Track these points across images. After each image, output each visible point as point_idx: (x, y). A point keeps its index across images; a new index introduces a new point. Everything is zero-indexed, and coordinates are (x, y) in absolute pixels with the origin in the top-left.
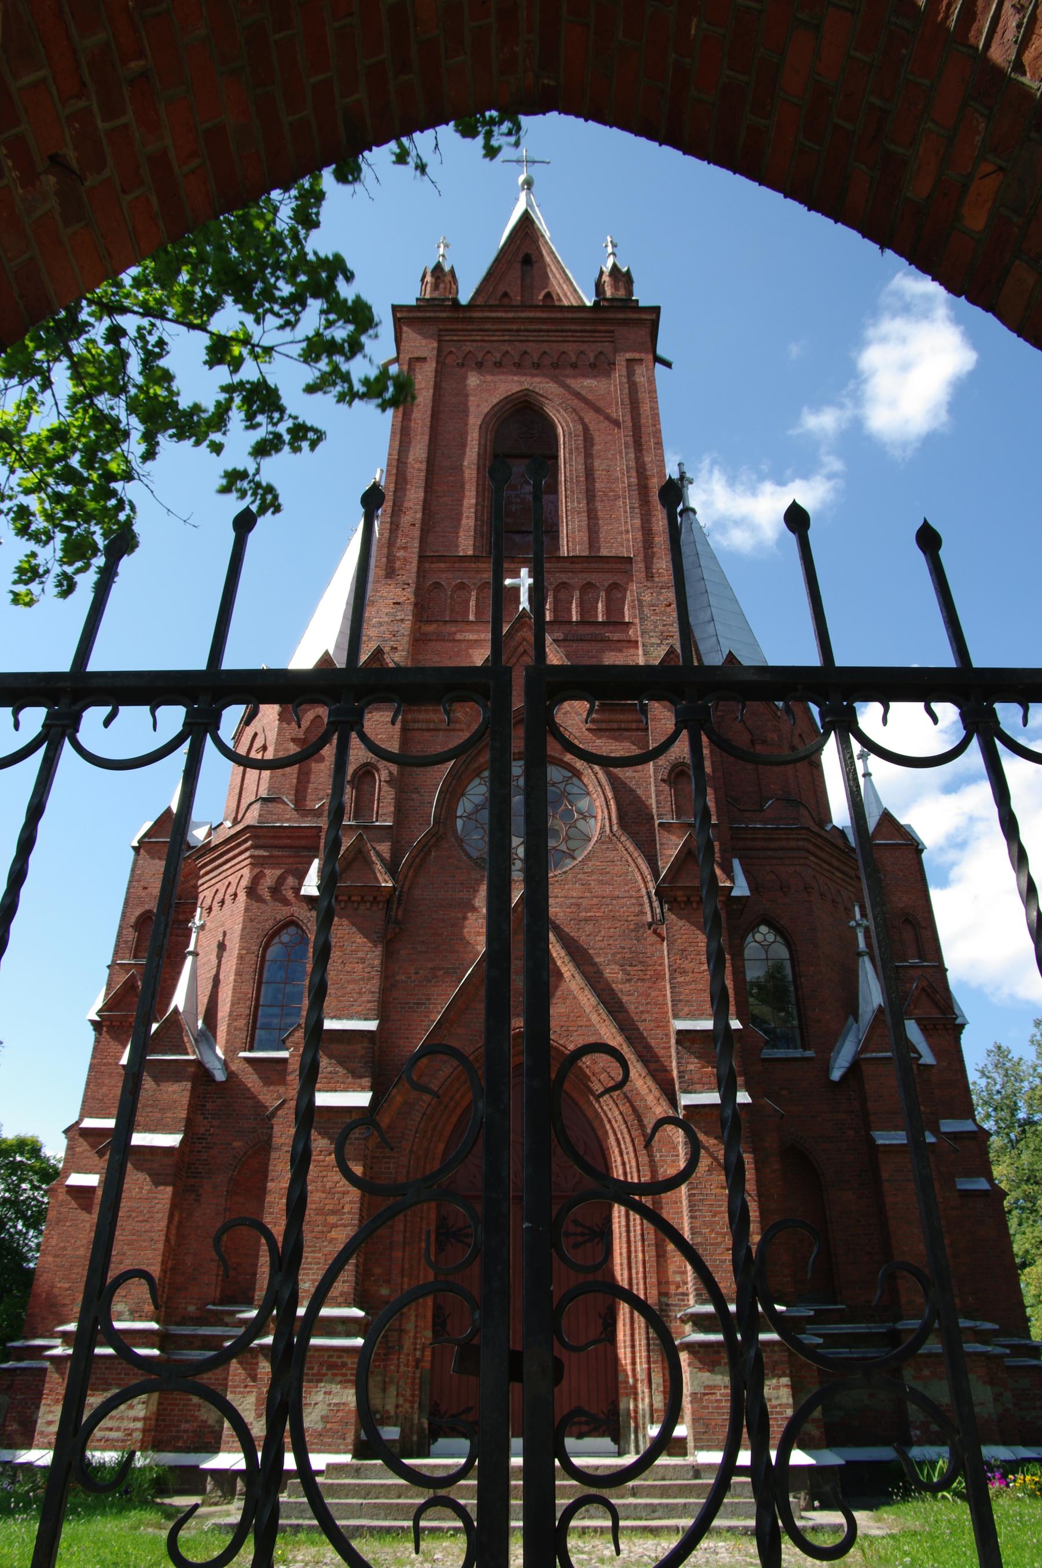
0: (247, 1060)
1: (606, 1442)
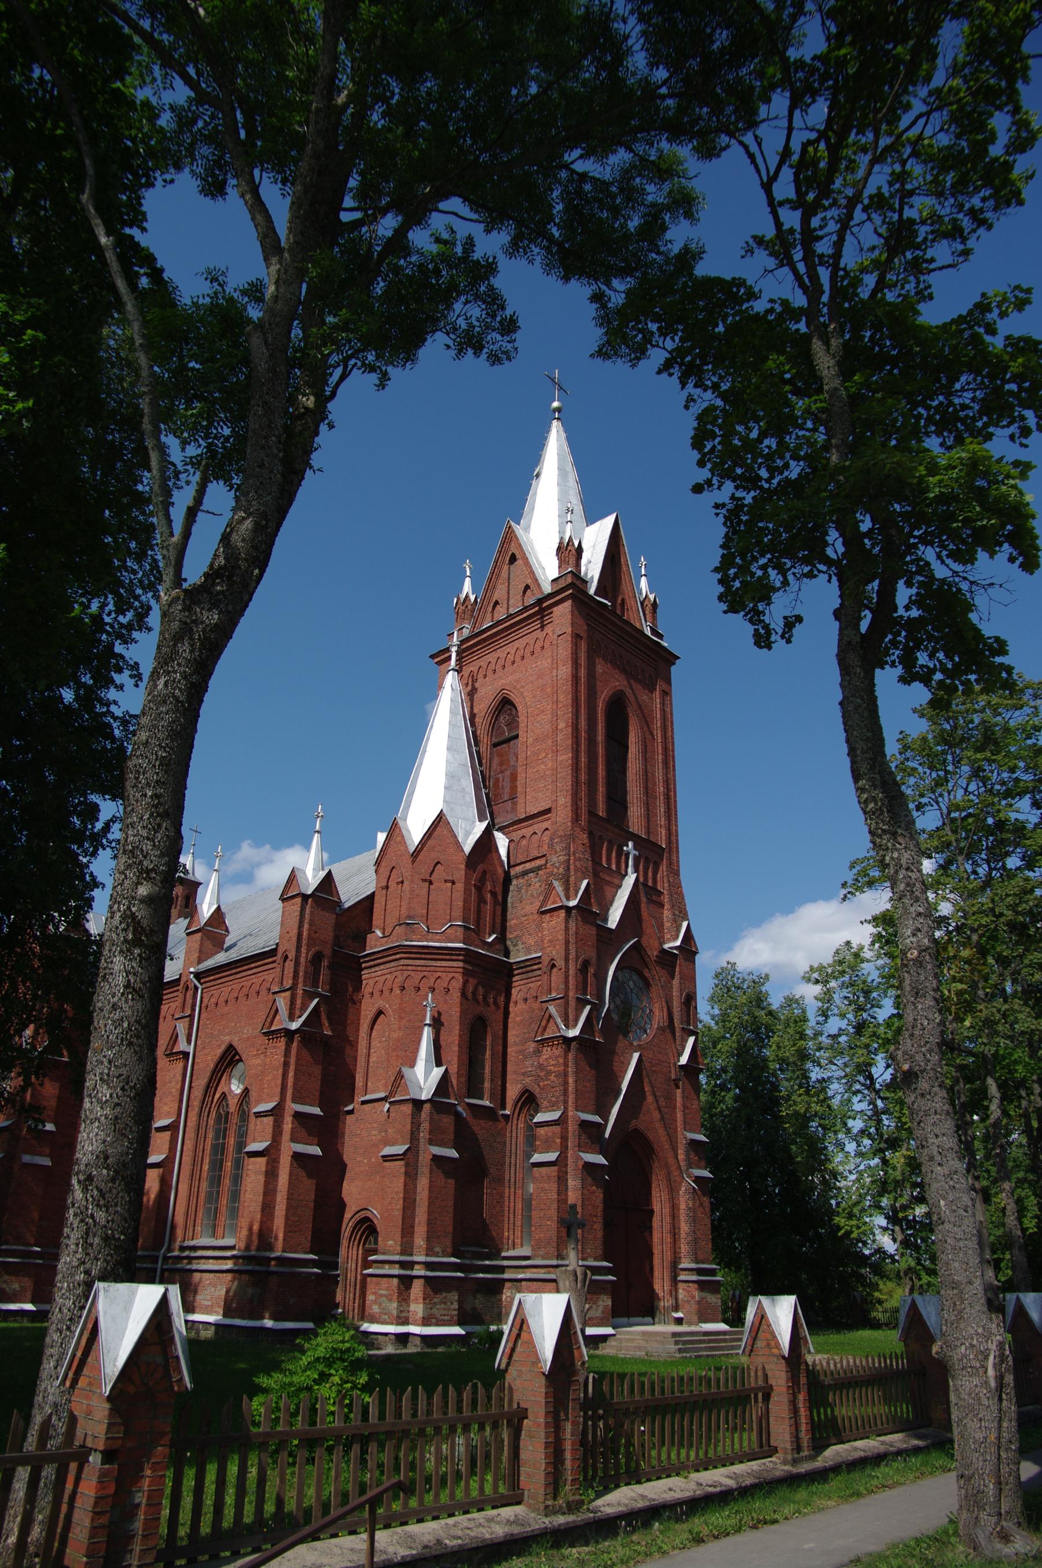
0: (468, 1104)
1: (650, 1319)
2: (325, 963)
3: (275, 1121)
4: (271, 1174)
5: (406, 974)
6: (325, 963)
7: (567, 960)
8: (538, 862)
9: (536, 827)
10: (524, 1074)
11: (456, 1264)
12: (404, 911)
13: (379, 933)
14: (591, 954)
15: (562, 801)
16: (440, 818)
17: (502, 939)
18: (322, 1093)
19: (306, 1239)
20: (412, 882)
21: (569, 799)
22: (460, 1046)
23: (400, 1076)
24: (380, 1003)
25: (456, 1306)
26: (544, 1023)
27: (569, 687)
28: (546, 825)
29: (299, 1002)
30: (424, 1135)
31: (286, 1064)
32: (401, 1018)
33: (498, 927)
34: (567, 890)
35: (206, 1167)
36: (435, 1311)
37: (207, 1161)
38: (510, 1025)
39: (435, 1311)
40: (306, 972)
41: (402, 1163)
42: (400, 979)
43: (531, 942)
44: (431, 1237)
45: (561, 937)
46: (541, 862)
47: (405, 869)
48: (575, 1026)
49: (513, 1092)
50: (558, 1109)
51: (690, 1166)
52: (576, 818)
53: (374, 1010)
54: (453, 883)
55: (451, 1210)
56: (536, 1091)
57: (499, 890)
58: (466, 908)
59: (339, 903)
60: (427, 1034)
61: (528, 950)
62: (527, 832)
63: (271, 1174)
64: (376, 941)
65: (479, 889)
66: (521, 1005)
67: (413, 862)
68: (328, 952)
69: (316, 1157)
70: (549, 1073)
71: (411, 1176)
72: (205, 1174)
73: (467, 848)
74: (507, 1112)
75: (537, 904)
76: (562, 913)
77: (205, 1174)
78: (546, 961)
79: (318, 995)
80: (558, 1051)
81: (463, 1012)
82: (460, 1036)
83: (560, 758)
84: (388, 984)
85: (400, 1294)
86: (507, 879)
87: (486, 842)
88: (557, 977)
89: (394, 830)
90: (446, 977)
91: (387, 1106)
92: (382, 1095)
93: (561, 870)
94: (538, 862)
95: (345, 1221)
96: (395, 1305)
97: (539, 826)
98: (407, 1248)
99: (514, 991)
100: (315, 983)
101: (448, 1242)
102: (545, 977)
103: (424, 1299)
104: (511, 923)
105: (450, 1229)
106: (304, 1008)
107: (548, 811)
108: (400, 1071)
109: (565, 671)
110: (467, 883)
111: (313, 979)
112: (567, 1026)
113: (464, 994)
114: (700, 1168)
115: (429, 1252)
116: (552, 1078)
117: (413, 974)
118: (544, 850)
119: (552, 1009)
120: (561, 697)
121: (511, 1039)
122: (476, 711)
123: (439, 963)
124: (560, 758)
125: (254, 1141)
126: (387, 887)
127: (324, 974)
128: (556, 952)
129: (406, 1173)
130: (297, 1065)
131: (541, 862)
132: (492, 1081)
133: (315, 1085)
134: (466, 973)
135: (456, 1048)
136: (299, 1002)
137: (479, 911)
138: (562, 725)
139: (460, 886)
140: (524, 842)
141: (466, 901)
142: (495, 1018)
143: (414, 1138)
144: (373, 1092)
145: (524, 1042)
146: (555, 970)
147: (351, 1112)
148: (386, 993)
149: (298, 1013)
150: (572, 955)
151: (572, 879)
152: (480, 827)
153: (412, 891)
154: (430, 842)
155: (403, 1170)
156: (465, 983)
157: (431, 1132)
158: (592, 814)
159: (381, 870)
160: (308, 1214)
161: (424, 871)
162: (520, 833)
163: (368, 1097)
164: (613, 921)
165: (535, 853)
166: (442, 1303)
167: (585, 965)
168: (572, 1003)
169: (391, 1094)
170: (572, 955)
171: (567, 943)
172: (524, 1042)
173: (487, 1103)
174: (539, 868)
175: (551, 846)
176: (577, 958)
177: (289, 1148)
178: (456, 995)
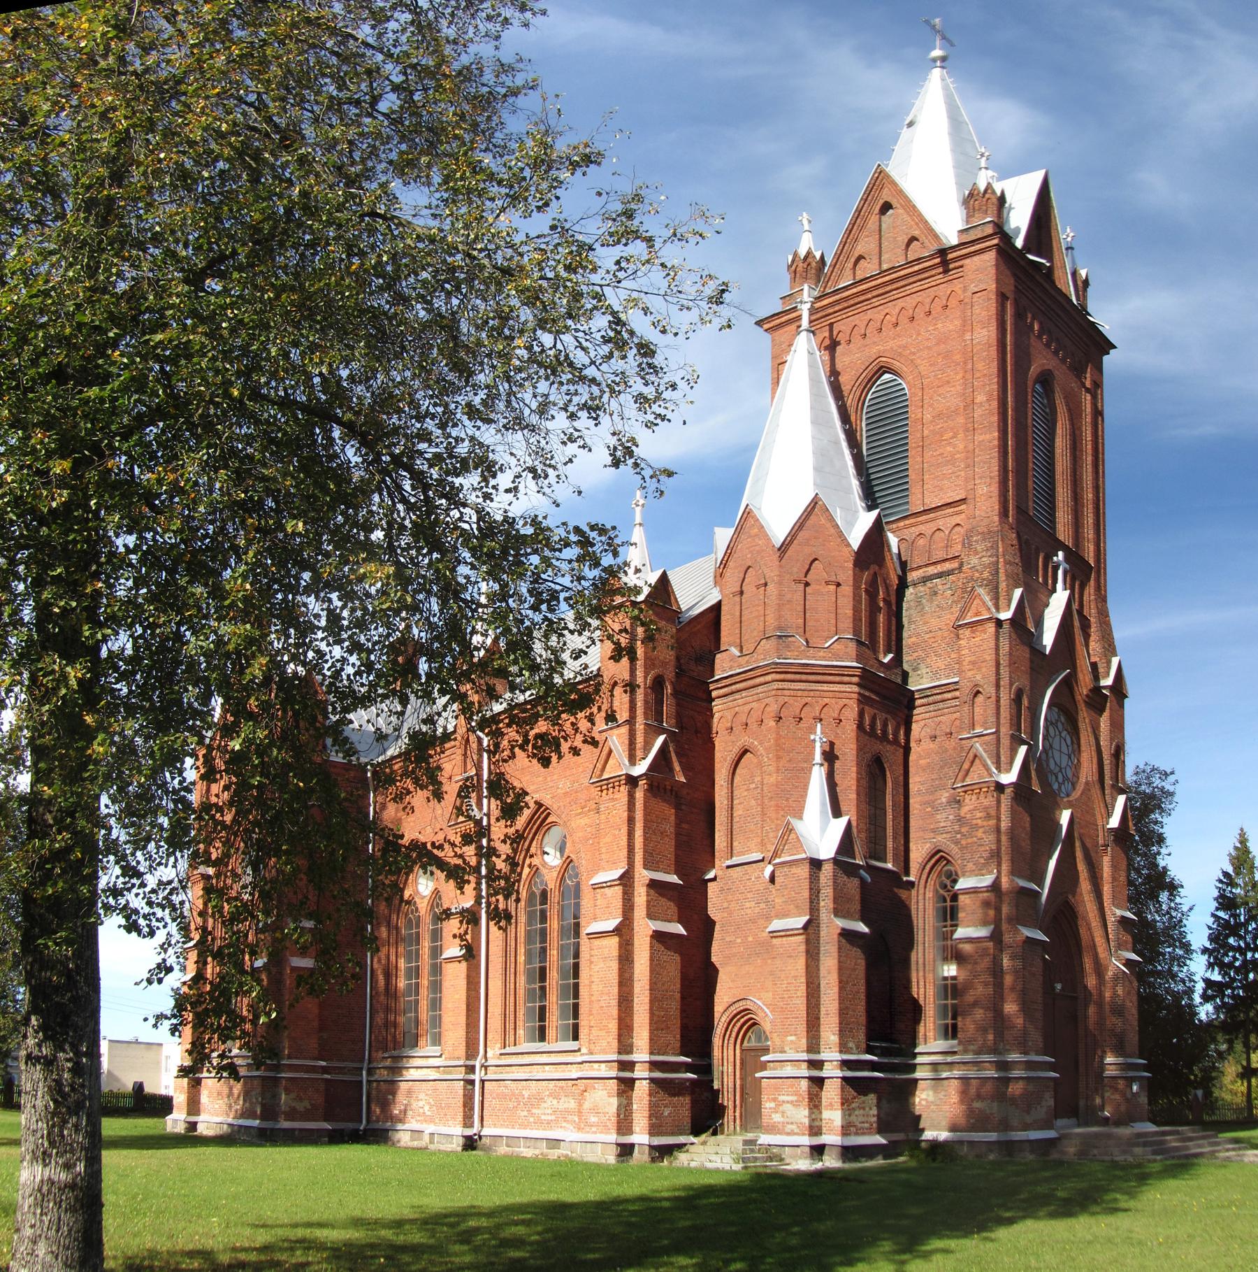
2: (669, 689)
3: (625, 893)
4: (626, 959)
5: (781, 700)
6: (669, 689)
7: (998, 686)
8: (948, 566)
9: (940, 523)
10: (933, 831)
11: (871, 1062)
12: (771, 620)
13: (735, 651)
14: (1024, 682)
15: (982, 490)
16: (815, 502)
17: (898, 660)
18: (677, 856)
19: (674, 1038)
20: (780, 583)
21: (995, 489)
22: (858, 794)
23: (789, 830)
24: (745, 740)
25: (874, 1111)
26: (966, 766)
27: (994, 352)
28: (957, 519)
29: (640, 739)
30: (826, 903)
31: (631, 821)
32: (778, 758)
33: (894, 648)
34: (996, 599)
35: (521, 958)
36: (853, 1118)
37: (521, 950)
38: (912, 770)
39: (853, 1118)
40: (646, 702)
41: (802, 938)
42: (773, 708)
43: (941, 664)
44: (844, 1030)
45: (989, 656)
46: (955, 564)
47: (770, 568)
48: (1009, 770)
49: (918, 853)
50: (991, 872)
51: (1120, 946)
52: (1004, 513)
53: (736, 750)
54: (838, 585)
55: (863, 997)
56: (954, 850)
57: (893, 599)
58: (856, 619)
59: (678, 613)
60: (818, 777)
61: (935, 675)
62: (927, 529)
63: (626, 959)
64: (725, 665)
65: (872, 594)
66: (927, 745)
67: (781, 558)
68: (670, 674)
69: (679, 936)
70: (977, 827)
71: (812, 954)
72: (521, 968)
73: (856, 548)
74: (912, 878)
75: (953, 618)
76: (991, 628)
77: (521, 968)
78: (966, 687)
79: (663, 731)
80: (989, 801)
81: (860, 750)
82: (858, 780)
83: (978, 438)
84: (755, 716)
85: (811, 1099)
86: (903, 585)
87: (875, 536)
88: (983, 707)
89: (747, 522)
90: (835, 705)
91: (769, 869)
92: (758, 856)
93: (986, 574)
94: (948, 566)
95: (717, 1015)
96: (806, 1112)
97: (946, 521)
98: (813, 1046)
99: (914, 726)
100: (658, 716)
101: (862, 1036)
102: (966, 708)
103: (842, 1104)
104: (906, 642)
105: (863, 1020)
106: (647, 750)
107: (963, 501)
108: (788, 823)
109: (985, 335)
110: (856, 587)
111: (655, 710)
112: (999, 768)
113: (860, 726)
114: (1127, 950)
115: (843, 1048)
116: (980, 834)
117: (791, 700)
118: (957, 549)
119: (979, 748)
120: (980, 366)
121: (913, 788)
122: (839, 367)
123: (825, 687)
124: (978, 438)
125: (595, 919)
126: (742, 593)
127: (668, 707)
128: (983, 676)
129: (807, 952)
130: (646, 821)
131: (955, 564)
132: (894, 838)
133: (668, 847)
134: (863, 701)
135: (854, 796)
136: (640, 739)
137: (873, 625)
138: (980, 398)
139: (847, 589)
140: (921, 542)
141: (856, 610)
142: (892, 756)
143: (814, 909)
144: (743, 853)
145: (933, 790)
146: (980, 699)
147: (714, 879)
148: (753, 726)
149: (639, 753)
150: (1005, 681)
151: (1003, 585)
152: (866, 520)
153: (780, 596)
154: (801, 534)
155: (803, 948)
156: (861, 714)
157: (835, 900)
158: (1021, 510)
159: (728, 573)
160: (674, 1006)
161: (797, 570)
162: (915, 531)
163: (735, 860)
164: (1048, 639)
165: (941, 555)
166: (860, 1108)
167: (1019, 695)
168: (1005, 742)
169: (776, 854)
170: (1005, 681)
171: (998, 665)
172: (933, 790)
173: (890, 866)
174: (950, 573)
175: (967, 543)
176: (1011, 685)
177: (644, 928)
178: (850, 728)
